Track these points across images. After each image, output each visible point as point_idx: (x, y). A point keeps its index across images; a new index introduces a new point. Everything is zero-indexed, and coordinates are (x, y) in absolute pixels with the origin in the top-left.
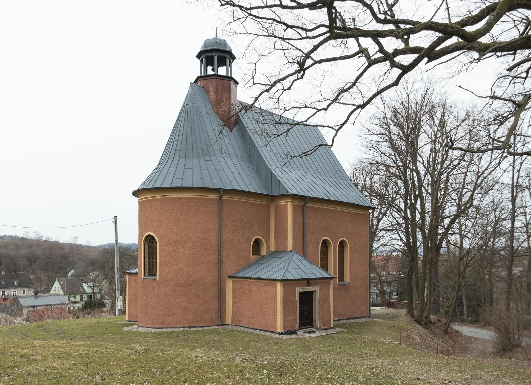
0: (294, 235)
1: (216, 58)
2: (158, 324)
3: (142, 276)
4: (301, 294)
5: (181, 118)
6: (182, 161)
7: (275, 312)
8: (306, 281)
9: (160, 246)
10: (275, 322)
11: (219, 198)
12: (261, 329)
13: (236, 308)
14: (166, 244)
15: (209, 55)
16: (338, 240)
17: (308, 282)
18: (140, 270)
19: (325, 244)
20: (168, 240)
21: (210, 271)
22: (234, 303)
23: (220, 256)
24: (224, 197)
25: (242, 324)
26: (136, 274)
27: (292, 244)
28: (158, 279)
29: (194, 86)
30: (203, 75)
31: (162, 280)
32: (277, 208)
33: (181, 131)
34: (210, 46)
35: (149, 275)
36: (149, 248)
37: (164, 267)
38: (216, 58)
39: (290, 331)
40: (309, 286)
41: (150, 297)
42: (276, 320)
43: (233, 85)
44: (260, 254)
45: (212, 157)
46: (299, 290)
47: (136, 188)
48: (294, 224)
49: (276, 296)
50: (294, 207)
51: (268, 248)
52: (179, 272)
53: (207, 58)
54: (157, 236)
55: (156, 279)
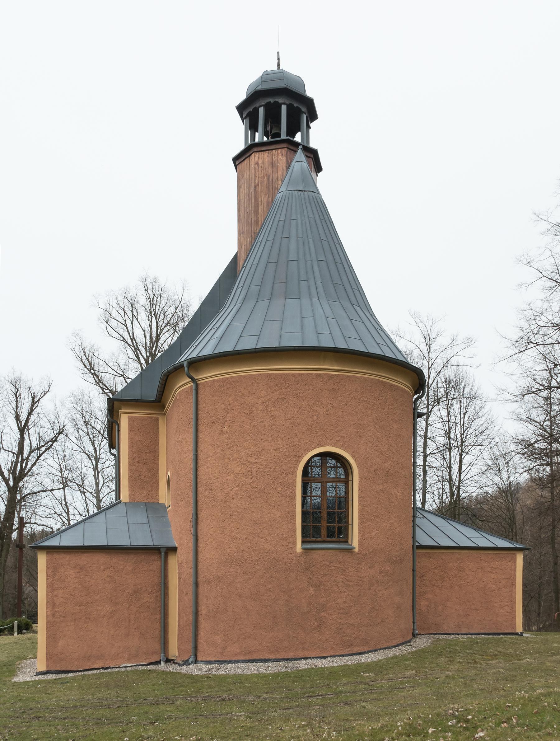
1: (284, 108)
7: (513, 602)
9: (361, 479)
10: (514, 618)
12: (486, 632)
15: (272, 100)
25: (445, 628)
30: (257, 140)
31: (364, 552)
37: (369, 523)
38: (284, 108)
49: (515, 575)
53: (268, 107)
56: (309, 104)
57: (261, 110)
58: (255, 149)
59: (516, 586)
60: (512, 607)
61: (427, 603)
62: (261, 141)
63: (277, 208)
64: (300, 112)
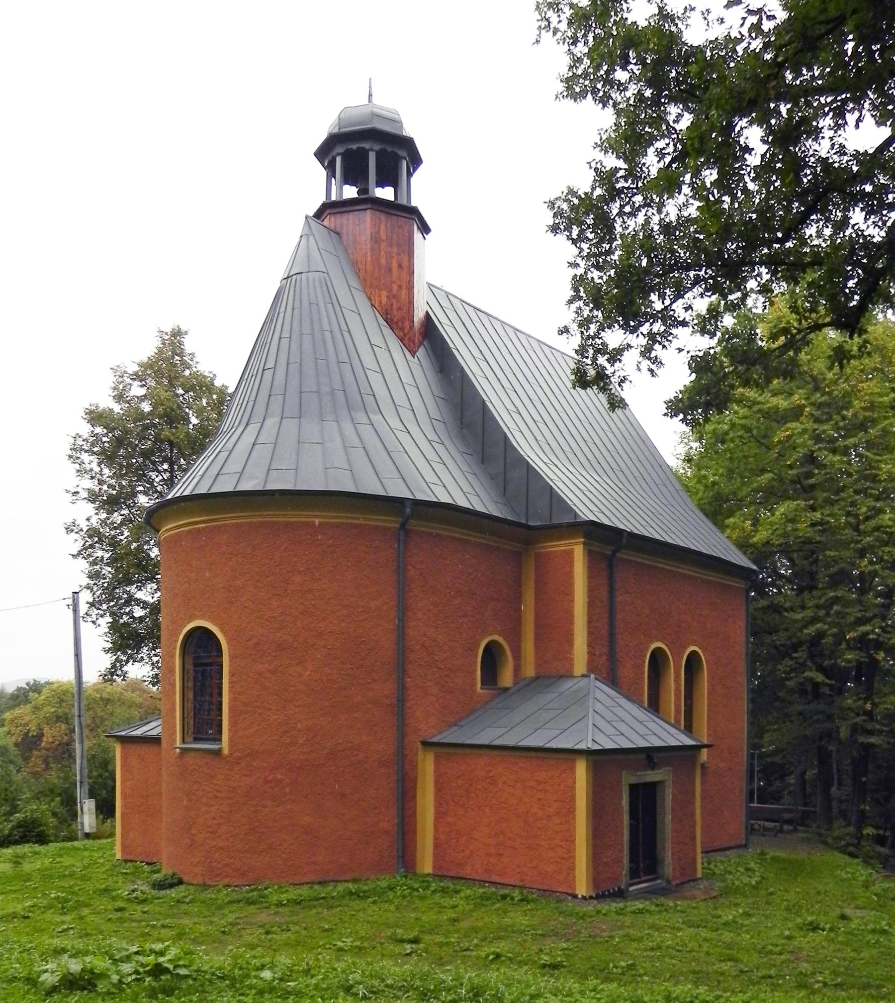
0: (590, 633)
1: (372, 157)
2: (227, 876)
3: (175, 740)
4: (633, 788)
5: (283, 309)
6: (290, 425)
7: (570, 840)
8: (643, 756)
9: (232, 657)
10: (572, 868)
11: (397, 526)
13: (447, 829)
14: (248, 651)
15: (354, 147)
16: (684, 652)
17: (649, 759)
18: (169, 727)
19: (657, 658)
20: (255, 640)
21: (376, 728)
22: (440, 815)
23: (402, 688)
24: (413, 524)
25: (467, 871)
26: (155, 741)
27: (586, 656)
28: (226, 751)
29: (314, 224)
30: (333, 198)
32: (541, 560)
33: (285, 342)
34: (360, 124)
35: (196, 740)
36: (195, 665)
37: (244, 716)
38: (372, 157)
39: (609, 891)
40: (653, 769)
41: (204, 800)
42: (574, 863)
43: (417, 235)
44: (496, 685)
45: (371, 416)
46: (628, 778)
47: (322, 137)
48: (591, 605)
50: (591, 556)
51: (517, 670)
52: (287, 732)
53: (346, 156)
54: (222, 630)
55: (220, 750)
56: (408, 144)
57: (339, 160)
58: (328, 211)
59: (575, 816)
60: (568, 850)
61: (447, 829)
62: (339, 199)
63: (254, 394)
64: (397, 159)
